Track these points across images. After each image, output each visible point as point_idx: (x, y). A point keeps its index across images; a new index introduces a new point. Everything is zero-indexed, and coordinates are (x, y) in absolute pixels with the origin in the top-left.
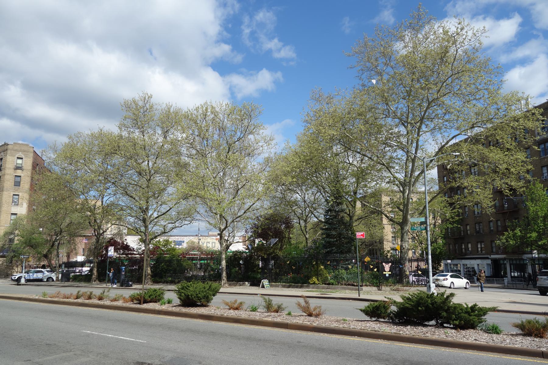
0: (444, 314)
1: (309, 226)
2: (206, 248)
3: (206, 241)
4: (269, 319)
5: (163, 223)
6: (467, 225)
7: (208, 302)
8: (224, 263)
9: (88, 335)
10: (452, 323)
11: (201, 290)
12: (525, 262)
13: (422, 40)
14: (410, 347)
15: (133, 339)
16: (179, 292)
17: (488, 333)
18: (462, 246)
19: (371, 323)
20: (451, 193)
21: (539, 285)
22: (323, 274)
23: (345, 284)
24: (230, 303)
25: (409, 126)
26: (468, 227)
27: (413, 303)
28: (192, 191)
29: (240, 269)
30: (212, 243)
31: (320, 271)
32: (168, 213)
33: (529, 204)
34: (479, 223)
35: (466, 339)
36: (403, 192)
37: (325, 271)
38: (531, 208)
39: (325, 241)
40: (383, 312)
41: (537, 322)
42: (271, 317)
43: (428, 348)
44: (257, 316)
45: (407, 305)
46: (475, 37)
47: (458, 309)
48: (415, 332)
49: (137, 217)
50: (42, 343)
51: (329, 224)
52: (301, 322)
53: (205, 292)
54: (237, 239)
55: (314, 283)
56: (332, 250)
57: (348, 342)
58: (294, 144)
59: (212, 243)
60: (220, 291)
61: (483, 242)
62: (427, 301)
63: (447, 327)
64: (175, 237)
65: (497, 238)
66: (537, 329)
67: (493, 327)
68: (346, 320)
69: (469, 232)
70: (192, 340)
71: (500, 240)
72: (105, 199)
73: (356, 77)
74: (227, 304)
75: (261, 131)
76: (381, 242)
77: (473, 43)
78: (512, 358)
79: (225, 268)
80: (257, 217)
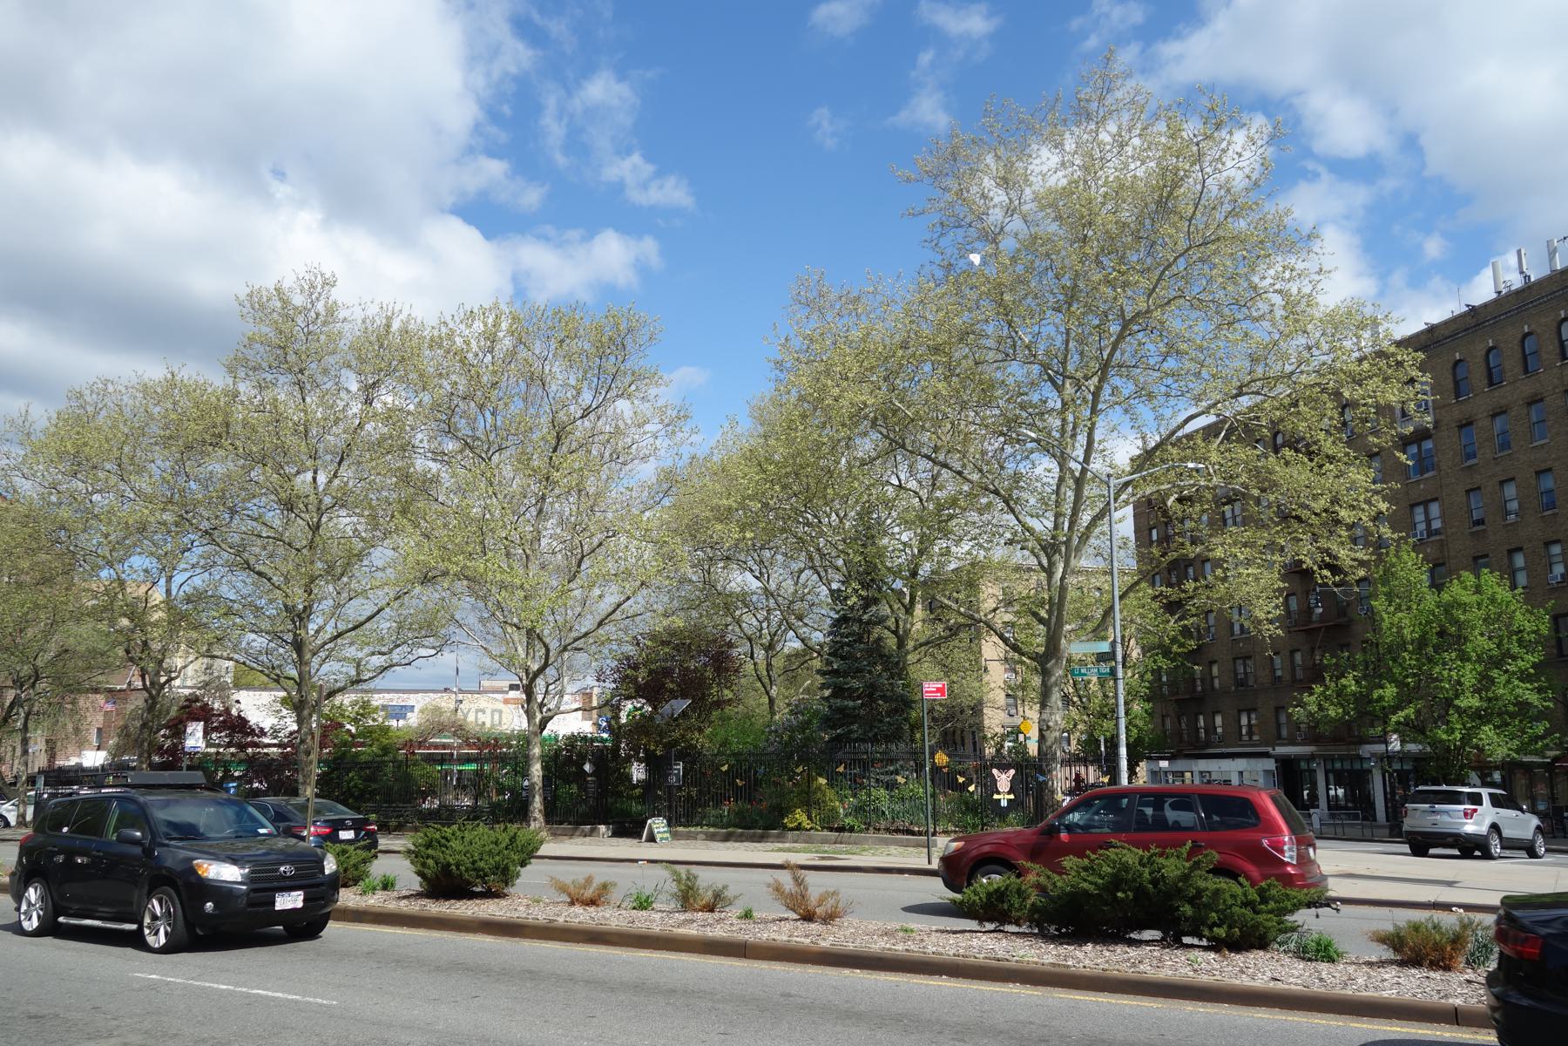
0: (1187, 909)
1: (778, 663)
2: (477, 729)
3: (474, 707)
4: (692, 931)
5: (351, 652)
6: (1212, 663)
7: (507, 885)
8: (536, 770)
9: (153, 987)
10: (1206, 932)
11: (487, 849)
12: (1365, 766)
13: (1108, 147)
14: (1097, 1002)
15: (296, 994)
16: (414, 855)
17: (1303, 959)
18: (1197, 720)
19: (984, 938)
20: (1170, 574)
21: (1409, 829)
22: (823, 802)
23: (887, 830)
24: (572, 887)
25: (1068, 385)
26: (1215, 670)
27: (1100, 881)
28: (449, 559)
29: (583, 787)
30: (493, 711)
31: (815, 793)
32: (367, 625)
33: (1379, 604)
34: (1247, 658)
35: (1248, 979)
36: (1049, 572)
37: (830, 794)
38: (1385, 616)
39: (830, 707)
40: (1016, 905)
41: (1435, 928)
42: (695, 924)
43: (1147, 1004)
44: (653, 922)
45: (1085, 885)
46: (1253, 148)
47: (1227, 896)
48: (1107, 962)
49: (275, 636)
50: (15, 1014)
51: (843, 658)
52: (785, 938)
53: (498, 854)
54: (570, 702)
55: (799, 828)
56: (851, 732)
57: (924, 993)
58: (746, 430)
59: (493, 711)
60: (540, 853)
61: (1255, 710)
62: (1141, 875)
63: (1192, 946)
64: (381, 695)
65: (1295, 698)
66: (1437, 947)
67: (1318, 944)
68: (912, 931)
69: (1217, 682)
70: (474, 994)
71: (1301, 704)
72: (179, 579)
73: (926, 241)
74: (563, 889)
75: (653, 391)
76: (977, 709)
77: (1248, 162)
78: (1376, 1027)
79: (540, 784)
80: (635, 638)
